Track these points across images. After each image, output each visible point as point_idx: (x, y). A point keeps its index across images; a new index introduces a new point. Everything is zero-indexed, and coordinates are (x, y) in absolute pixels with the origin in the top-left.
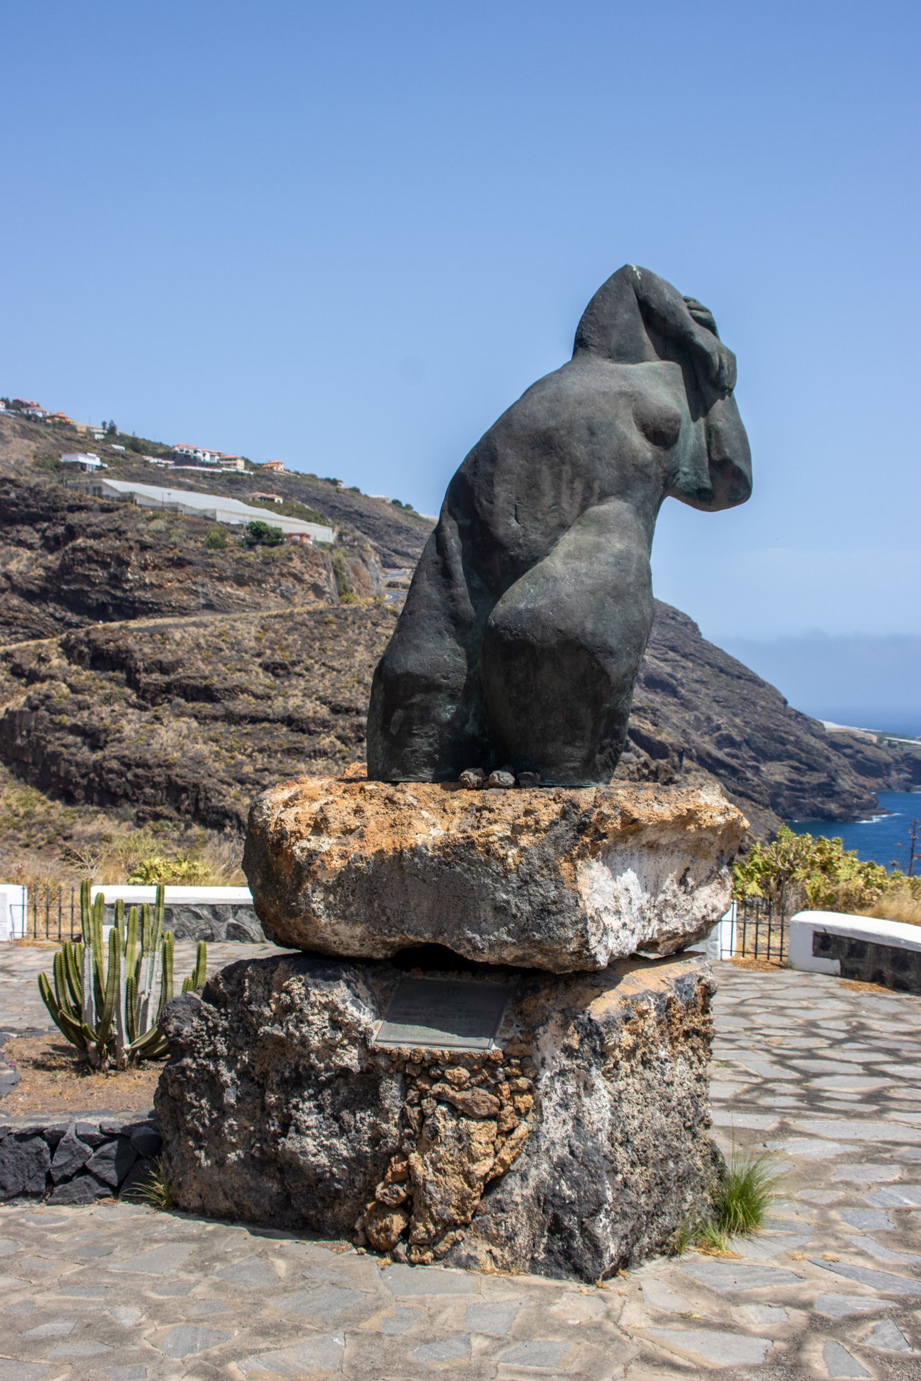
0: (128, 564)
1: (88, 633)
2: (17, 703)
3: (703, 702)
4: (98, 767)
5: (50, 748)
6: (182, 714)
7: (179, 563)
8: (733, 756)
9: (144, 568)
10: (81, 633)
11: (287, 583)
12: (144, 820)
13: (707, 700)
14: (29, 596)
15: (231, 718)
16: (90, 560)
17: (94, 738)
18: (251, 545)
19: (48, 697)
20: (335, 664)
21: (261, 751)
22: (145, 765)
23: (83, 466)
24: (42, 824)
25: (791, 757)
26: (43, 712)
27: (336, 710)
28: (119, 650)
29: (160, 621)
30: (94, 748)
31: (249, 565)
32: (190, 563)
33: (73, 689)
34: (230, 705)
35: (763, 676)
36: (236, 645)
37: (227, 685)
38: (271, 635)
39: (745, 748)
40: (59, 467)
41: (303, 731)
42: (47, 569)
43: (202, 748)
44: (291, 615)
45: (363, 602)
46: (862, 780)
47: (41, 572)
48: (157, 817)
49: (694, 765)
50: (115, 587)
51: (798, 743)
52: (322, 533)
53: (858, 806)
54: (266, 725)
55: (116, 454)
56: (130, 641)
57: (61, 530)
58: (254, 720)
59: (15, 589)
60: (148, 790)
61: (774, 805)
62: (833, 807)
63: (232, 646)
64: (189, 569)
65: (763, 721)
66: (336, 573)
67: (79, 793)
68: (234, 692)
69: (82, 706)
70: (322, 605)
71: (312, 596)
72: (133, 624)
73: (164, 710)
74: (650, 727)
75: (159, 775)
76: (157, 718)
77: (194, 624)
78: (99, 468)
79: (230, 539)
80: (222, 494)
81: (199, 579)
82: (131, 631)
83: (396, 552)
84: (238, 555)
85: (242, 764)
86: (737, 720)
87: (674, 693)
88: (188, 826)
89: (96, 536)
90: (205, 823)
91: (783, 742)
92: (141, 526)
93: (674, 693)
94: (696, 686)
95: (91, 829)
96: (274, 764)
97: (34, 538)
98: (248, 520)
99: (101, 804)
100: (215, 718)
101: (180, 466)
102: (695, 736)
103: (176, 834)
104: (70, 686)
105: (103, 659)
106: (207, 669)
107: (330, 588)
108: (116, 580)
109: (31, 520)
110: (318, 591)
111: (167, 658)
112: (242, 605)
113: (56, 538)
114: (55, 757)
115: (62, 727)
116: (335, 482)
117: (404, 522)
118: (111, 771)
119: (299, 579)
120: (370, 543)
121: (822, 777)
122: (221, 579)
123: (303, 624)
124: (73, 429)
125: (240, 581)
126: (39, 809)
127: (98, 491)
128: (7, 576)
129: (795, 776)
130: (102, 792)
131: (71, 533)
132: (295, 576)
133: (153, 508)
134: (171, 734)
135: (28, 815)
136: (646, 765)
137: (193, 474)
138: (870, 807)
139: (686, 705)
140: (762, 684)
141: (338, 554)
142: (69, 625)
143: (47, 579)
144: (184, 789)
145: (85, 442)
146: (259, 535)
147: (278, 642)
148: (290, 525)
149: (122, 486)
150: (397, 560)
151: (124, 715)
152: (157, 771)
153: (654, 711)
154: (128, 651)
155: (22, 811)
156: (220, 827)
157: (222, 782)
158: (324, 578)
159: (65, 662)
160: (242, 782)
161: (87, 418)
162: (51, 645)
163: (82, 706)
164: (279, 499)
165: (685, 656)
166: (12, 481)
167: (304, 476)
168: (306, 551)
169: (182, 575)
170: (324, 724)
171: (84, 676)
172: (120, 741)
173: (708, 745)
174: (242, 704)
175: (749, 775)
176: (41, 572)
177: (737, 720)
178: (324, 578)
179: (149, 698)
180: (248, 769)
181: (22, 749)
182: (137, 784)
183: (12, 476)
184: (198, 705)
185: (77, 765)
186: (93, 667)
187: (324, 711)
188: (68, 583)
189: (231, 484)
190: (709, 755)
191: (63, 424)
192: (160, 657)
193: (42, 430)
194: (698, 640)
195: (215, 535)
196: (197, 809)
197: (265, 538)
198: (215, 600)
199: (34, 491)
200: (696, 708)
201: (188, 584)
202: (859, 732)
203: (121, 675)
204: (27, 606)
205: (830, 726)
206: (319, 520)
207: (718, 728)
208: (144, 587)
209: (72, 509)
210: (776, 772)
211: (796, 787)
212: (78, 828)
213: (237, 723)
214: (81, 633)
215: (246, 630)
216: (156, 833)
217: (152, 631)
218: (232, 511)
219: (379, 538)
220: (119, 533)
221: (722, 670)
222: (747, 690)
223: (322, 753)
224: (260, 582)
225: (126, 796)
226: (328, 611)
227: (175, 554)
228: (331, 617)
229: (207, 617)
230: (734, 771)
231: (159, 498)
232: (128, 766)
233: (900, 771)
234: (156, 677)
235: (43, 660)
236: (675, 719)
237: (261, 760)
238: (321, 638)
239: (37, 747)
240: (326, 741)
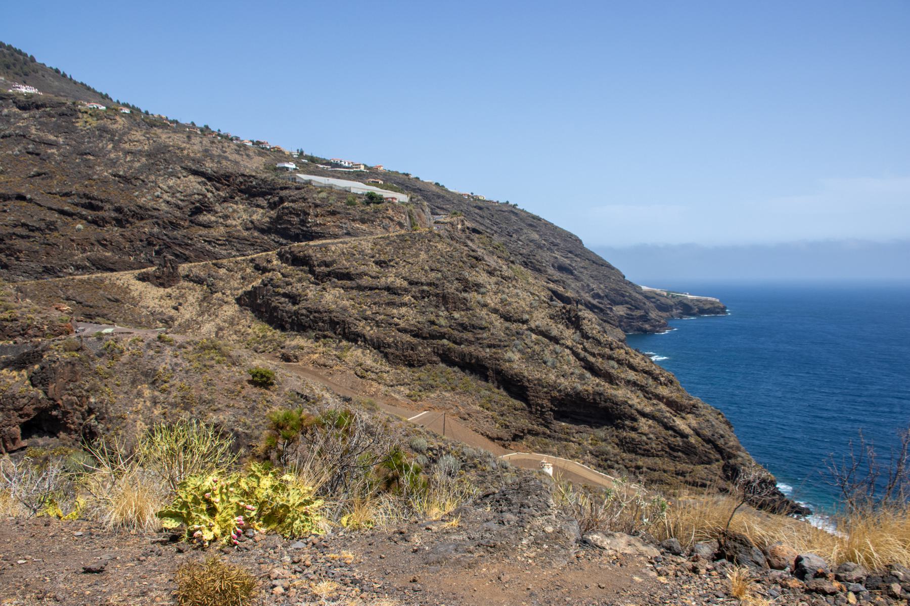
0: (309, 214)
1: (290, 248)
2: (257, 283)
3: (585, 277)
4: (296, 313)
5: (273, 304)
6: (336, 287)
7: (333, 213)
9: (317, 216)
10: (287, 248)
11: (386, 221)
12: (319, 338)
13: (587, 277)
14: (262, 231)
15: (360, 288)
16: (291, 213)
17: (294, 299)
18: (368, 204)
19: (272, 280)
20: (410, 261)
21: (375, 304)
22: (318, 312)
23: (287, 169)
24: (271, 341)
25: (627, 303)
26: (269, 287)
27: (411, 283)
28: (305, 256)
29: (324, 241)
30: (294, 304)
31: (367, 213)
32: (339, 213)
33: (284, 275)
34: (359, 281)
35: (613, 264)
36: (362, 252)
37: (357, 272)
38: (379, 247)
39: (605, 299)
40: (276, 169)
41: (395, 294)
42: (270, 218)
43: (346, 303)
44: (388, 237)
45: (423, 230)
46: (660, 313)
47: (268, 219)
48: (325, 337)
49: (583, 308)
50: (303, 226)
51: (630, 296)
52: (402, 198)
53: (659, 326)
54: (377, 291)
55: (304, 163)
56: (310, 251)
57: (277, 199)
58: (371, 289)
59: (256, 228)
60: (320, 324)
61: (620, 326)
62: (647, 326)
63: (360, 253)
64: (338, 216)
65: (614, 286)
66: (410, 217)
67: (288, 326)
68: (361, 275)
69: (288, 284)
70: (403, 232)
71: (398, 228)
72: (311, 243)
73: (327, 284)
74: (562, 289)
75: (326, 317)
76: (324, 289)
77: (341, 242)
78: (295, 169)
79: (358, 201)
80: (354, 180)
81: (343, 220)
82: (311, 247)
83: (438, 207)
84: (362, 208)
85: (366, 310)
86: (602, 286)
87: (572, 273)
88: (340, 341)
89: (293, 201)
90: (348, 340)
91: (623, 296)
92: (315, 195)
93: (572, 273)
94: (582, 270)
95: (294, 343)
96: (381, 310)
97: (264, 203)
98: (366, 192)
99: (298, 331)
100: (352, 288)
101: (334, 168)
102: (582, 294)
103: (334, 345)
104: (282, 274)
105: (298, 261)
106: (347, 264)
107: (407, 224)
108: (303, 222)
109: (263, 195)
110: (401, 225)
111: (328, 259)
112: (364, 233)
113: (275, 203)
114: (276, 308)
115: (278, 294)
116: (407, 175)
117: (442, 193)
118: (302, 315)
119: (392, 220)
120: (425, 203)
121: (642, 313)
122: (353, 220)
123: (394, 241)
124: (284, 153)
125: (363, 221)
126: (269, 334)
127: (294, 179)
128: (252, 222)
129: (629, 312)
130: (299, 326)
131: (282, 200)
132: (389, 218)
133: (320, 187)
134: (331, 296)
135: (264, 337)
136: (564, 308)
137: (340, 172)
138: (664, 326)
139: (577, 279)
140: (613, 268)
141: (410, 207)
142: (281, 244)
143: (271, 223)
144: (338, 323)
145: (289, 158)
146: (371, 198)
147: (382, 251)
148: (387, 194)
149: (305, 177)
150: (438, 211)
151: (308, 287)
152: (325, 314)
153: (564, 282)
154: (309, 256)
155: (261, 335)
156: (356, 342)
157: (356, 319)
158: (404, 219)
159: (279, 263)
160: (366, 319)
161: (289, 148)
162: (272, 254)
163: (288, 284)
164: (381, 182)
165: (576, 255)
166: (253, 176)
167: (393, 172)
168: (395, 206)
169: (335, 219)
170: (406, 290)
171: (289, 269)
172: (307, 300)
173: (587, 297)
174: (365, 281)
176: (268, 219)
177: (602, 286)
178: (404, 219)
179: (320, 279)
180: (369, 313)
181: (260, 305)
182: (315, 321)
183: (254, 174)
184: (344, 282)
185: (286, 312)
186: (293, 264)
187: (405, 284)
188: (280, 224)
189: (359, 176)
190: (589, 302)
191: (279, 151)
192: (325, 259)
193: (268, 152)
194: (583, 248)
195: (350, 199)
196: (344, 333)
197: (375, 200)
199: (264, 181)
200: (582, 280)
201: (338, 223)
202: (658, 291)
203: (306, 268)
204: (261, 236)
205: (644, 288)
206: (401, 191)
207: (593, 290)
208: (317, 225)
209: (282, 189)
210: (620, 310)
211: (630, 317)
212: (288, 343)
213: (363, 290)
214: (287, 248)
215: (366, 245)
216: (325, 344)
217: (321, 247)
218: (359, 188)
219: (429, 201)
220: (304, 199)
222: (605, 271)
223: (405, 305)
224: (373, 221)
225: (310, 327)
226: (406, 235)
227: (331, 209)
228: (408, 238)
229: (347, 239)
230: (601, 310)
231: (323, 182)
232: (311, 312)
233: (677, 309)
234: (323, 269)
235: (269, 262)
236: (573, 285)
237: (375, 308)
238: (403, 248)
239: (267, 304)
240: (407, 298)
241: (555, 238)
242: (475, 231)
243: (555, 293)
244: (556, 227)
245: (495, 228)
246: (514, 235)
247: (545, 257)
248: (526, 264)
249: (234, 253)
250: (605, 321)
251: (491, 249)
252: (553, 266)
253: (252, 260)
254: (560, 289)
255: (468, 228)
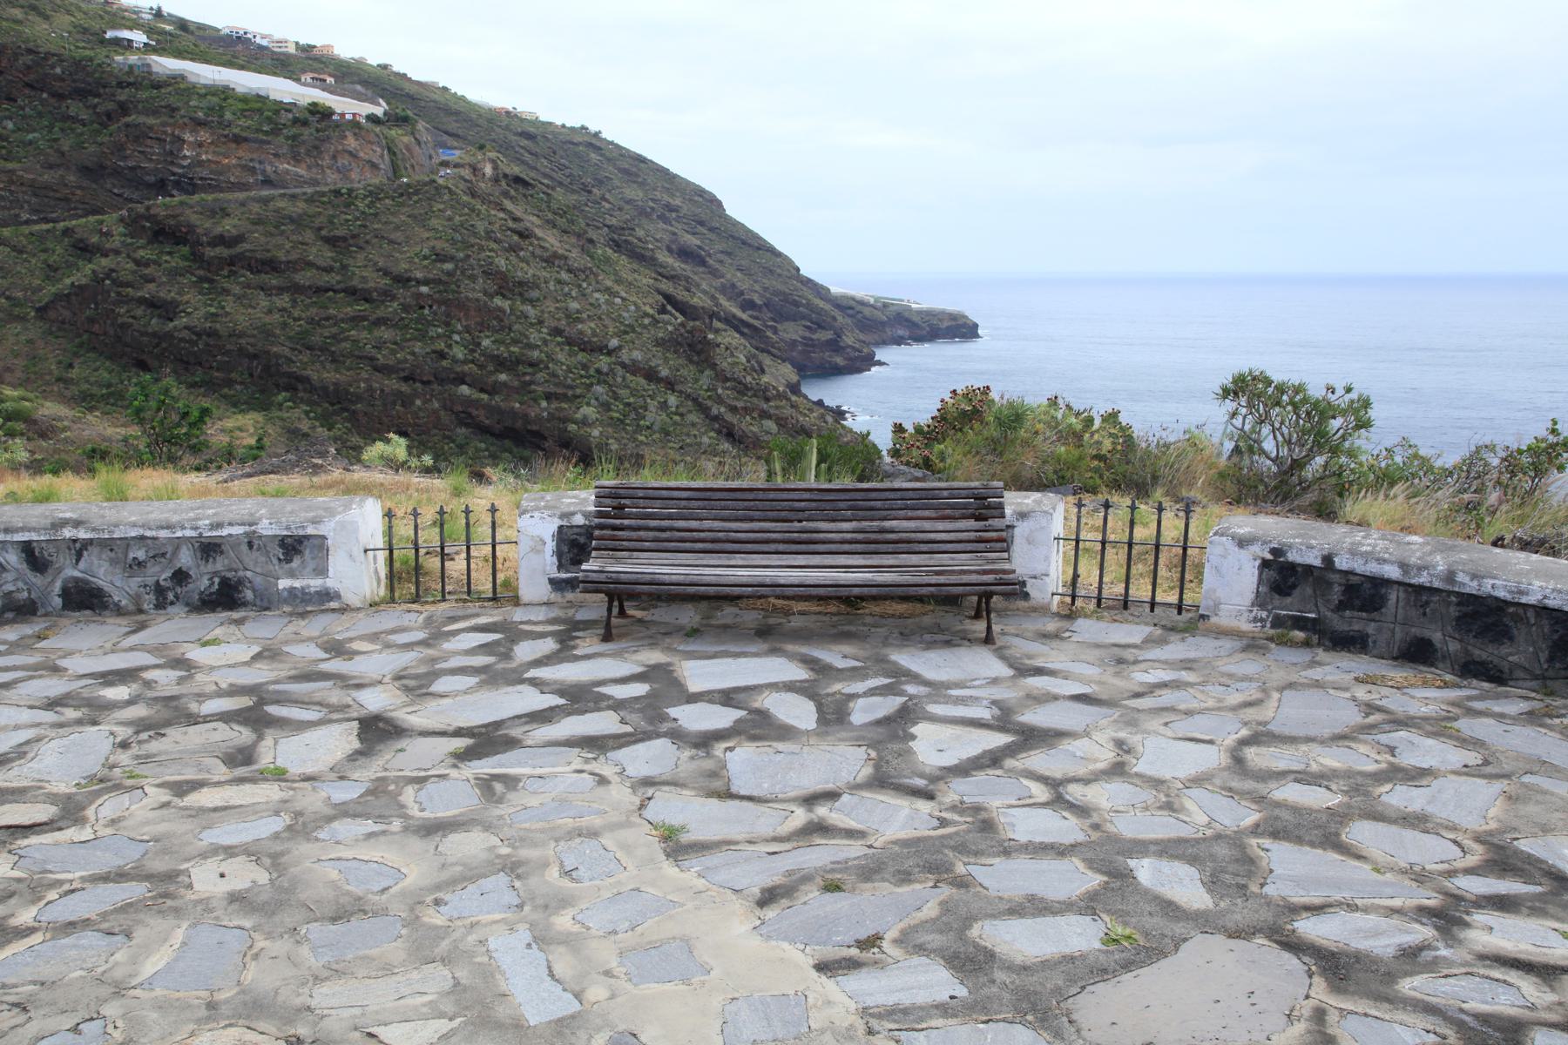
8: (756, 318)
25: (803, 317)
51: (809, 305)
57: (111, 106)
62: (839, 360)
66: (389, 149)
87: (703, 263)
91: (796, 304)
93: (703, 263)
101: (235, 49)
107: (384, 165)
109: (82, 94)
129: (807, 334)
131: (124, 109)
153: (687, 279)
175: (769, 334)
198: (273, 176)
221: (744, 243)
241: (672, 196)
242: (518, 180)
243: (669, 298)
244: (675, 176)
245: (559, 176)
246: (595, 190)
247: (652, 233)
248: (618, 245)
249: (25, 216)
250: (763, 351)
251: (550, 216)
252: (669, 250)
253: (67, 232)
254: (681, 294)
255: (505, 176)
